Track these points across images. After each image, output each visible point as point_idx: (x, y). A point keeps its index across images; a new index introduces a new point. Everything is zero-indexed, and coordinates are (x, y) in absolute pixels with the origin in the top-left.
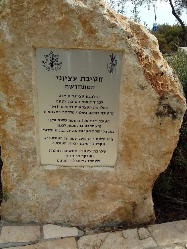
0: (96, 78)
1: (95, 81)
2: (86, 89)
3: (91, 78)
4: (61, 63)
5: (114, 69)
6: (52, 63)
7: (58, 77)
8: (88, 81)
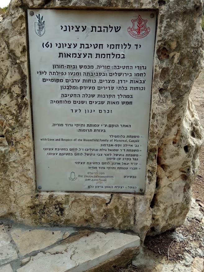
0: (96, 44)
1: (95, 48)
3: (91, 45)
4: (149, 28)
5: (42, 33)
6: (139, 28)
7: (62, 27)
8: (88, 48)
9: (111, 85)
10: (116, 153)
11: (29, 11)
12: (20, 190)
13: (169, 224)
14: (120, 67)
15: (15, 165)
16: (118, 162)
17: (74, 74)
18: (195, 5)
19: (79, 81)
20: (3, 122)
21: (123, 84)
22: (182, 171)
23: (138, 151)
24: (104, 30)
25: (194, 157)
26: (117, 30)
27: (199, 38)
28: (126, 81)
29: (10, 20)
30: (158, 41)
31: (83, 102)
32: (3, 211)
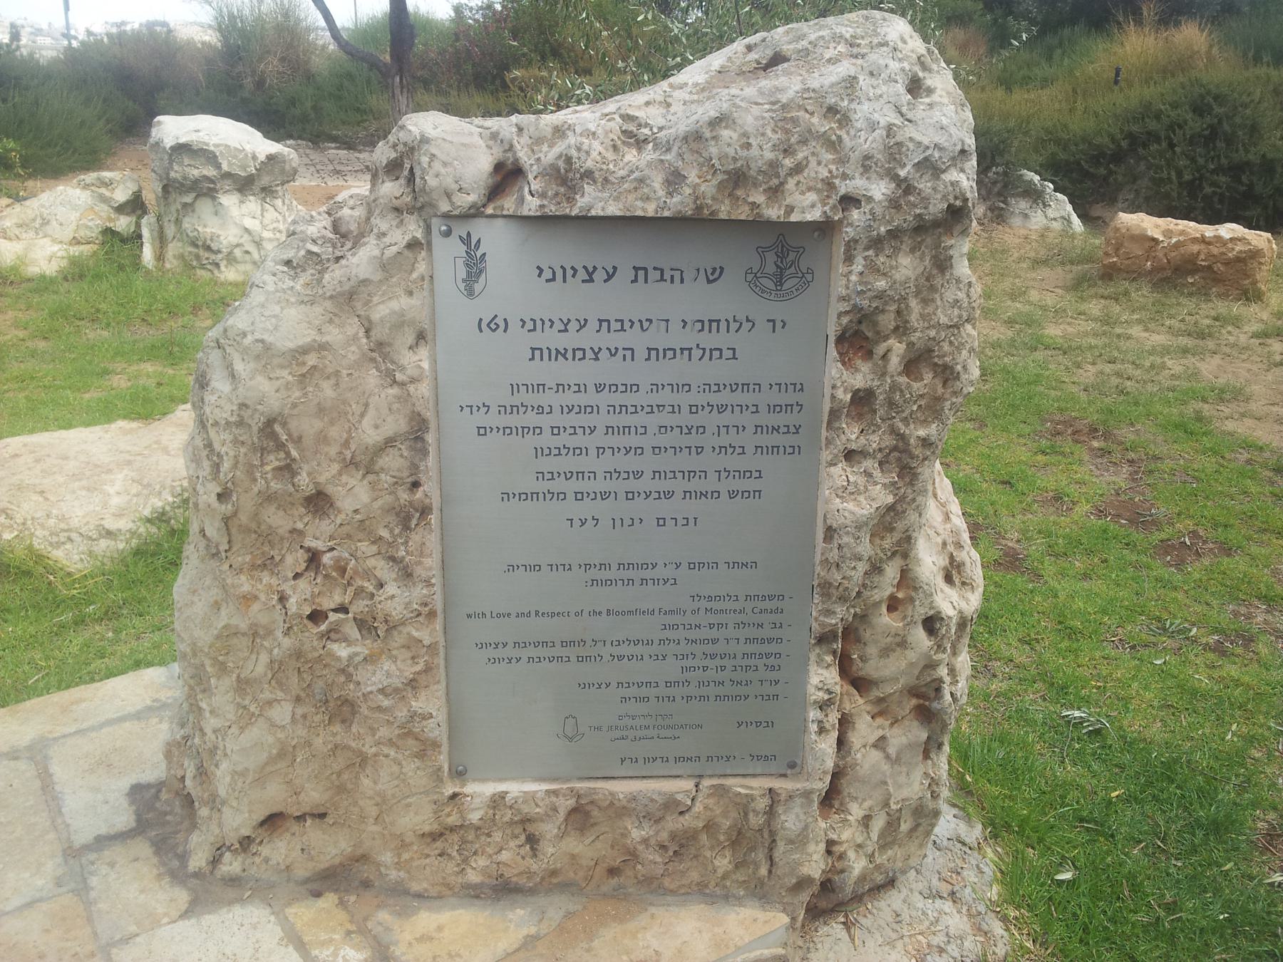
3: (575, 270)
9: (694, 440)
10: (710, 648)
12: (396, 782)
13: (878, 867)
15: (386, 703)
16: (721, 676)
19: (592, 432)
22: (917, 696)
26: (711, 278)
27: (961, 295)
29: (377, 252)
30: (840, 315)
31: (605, 496)
32: (334, 852)
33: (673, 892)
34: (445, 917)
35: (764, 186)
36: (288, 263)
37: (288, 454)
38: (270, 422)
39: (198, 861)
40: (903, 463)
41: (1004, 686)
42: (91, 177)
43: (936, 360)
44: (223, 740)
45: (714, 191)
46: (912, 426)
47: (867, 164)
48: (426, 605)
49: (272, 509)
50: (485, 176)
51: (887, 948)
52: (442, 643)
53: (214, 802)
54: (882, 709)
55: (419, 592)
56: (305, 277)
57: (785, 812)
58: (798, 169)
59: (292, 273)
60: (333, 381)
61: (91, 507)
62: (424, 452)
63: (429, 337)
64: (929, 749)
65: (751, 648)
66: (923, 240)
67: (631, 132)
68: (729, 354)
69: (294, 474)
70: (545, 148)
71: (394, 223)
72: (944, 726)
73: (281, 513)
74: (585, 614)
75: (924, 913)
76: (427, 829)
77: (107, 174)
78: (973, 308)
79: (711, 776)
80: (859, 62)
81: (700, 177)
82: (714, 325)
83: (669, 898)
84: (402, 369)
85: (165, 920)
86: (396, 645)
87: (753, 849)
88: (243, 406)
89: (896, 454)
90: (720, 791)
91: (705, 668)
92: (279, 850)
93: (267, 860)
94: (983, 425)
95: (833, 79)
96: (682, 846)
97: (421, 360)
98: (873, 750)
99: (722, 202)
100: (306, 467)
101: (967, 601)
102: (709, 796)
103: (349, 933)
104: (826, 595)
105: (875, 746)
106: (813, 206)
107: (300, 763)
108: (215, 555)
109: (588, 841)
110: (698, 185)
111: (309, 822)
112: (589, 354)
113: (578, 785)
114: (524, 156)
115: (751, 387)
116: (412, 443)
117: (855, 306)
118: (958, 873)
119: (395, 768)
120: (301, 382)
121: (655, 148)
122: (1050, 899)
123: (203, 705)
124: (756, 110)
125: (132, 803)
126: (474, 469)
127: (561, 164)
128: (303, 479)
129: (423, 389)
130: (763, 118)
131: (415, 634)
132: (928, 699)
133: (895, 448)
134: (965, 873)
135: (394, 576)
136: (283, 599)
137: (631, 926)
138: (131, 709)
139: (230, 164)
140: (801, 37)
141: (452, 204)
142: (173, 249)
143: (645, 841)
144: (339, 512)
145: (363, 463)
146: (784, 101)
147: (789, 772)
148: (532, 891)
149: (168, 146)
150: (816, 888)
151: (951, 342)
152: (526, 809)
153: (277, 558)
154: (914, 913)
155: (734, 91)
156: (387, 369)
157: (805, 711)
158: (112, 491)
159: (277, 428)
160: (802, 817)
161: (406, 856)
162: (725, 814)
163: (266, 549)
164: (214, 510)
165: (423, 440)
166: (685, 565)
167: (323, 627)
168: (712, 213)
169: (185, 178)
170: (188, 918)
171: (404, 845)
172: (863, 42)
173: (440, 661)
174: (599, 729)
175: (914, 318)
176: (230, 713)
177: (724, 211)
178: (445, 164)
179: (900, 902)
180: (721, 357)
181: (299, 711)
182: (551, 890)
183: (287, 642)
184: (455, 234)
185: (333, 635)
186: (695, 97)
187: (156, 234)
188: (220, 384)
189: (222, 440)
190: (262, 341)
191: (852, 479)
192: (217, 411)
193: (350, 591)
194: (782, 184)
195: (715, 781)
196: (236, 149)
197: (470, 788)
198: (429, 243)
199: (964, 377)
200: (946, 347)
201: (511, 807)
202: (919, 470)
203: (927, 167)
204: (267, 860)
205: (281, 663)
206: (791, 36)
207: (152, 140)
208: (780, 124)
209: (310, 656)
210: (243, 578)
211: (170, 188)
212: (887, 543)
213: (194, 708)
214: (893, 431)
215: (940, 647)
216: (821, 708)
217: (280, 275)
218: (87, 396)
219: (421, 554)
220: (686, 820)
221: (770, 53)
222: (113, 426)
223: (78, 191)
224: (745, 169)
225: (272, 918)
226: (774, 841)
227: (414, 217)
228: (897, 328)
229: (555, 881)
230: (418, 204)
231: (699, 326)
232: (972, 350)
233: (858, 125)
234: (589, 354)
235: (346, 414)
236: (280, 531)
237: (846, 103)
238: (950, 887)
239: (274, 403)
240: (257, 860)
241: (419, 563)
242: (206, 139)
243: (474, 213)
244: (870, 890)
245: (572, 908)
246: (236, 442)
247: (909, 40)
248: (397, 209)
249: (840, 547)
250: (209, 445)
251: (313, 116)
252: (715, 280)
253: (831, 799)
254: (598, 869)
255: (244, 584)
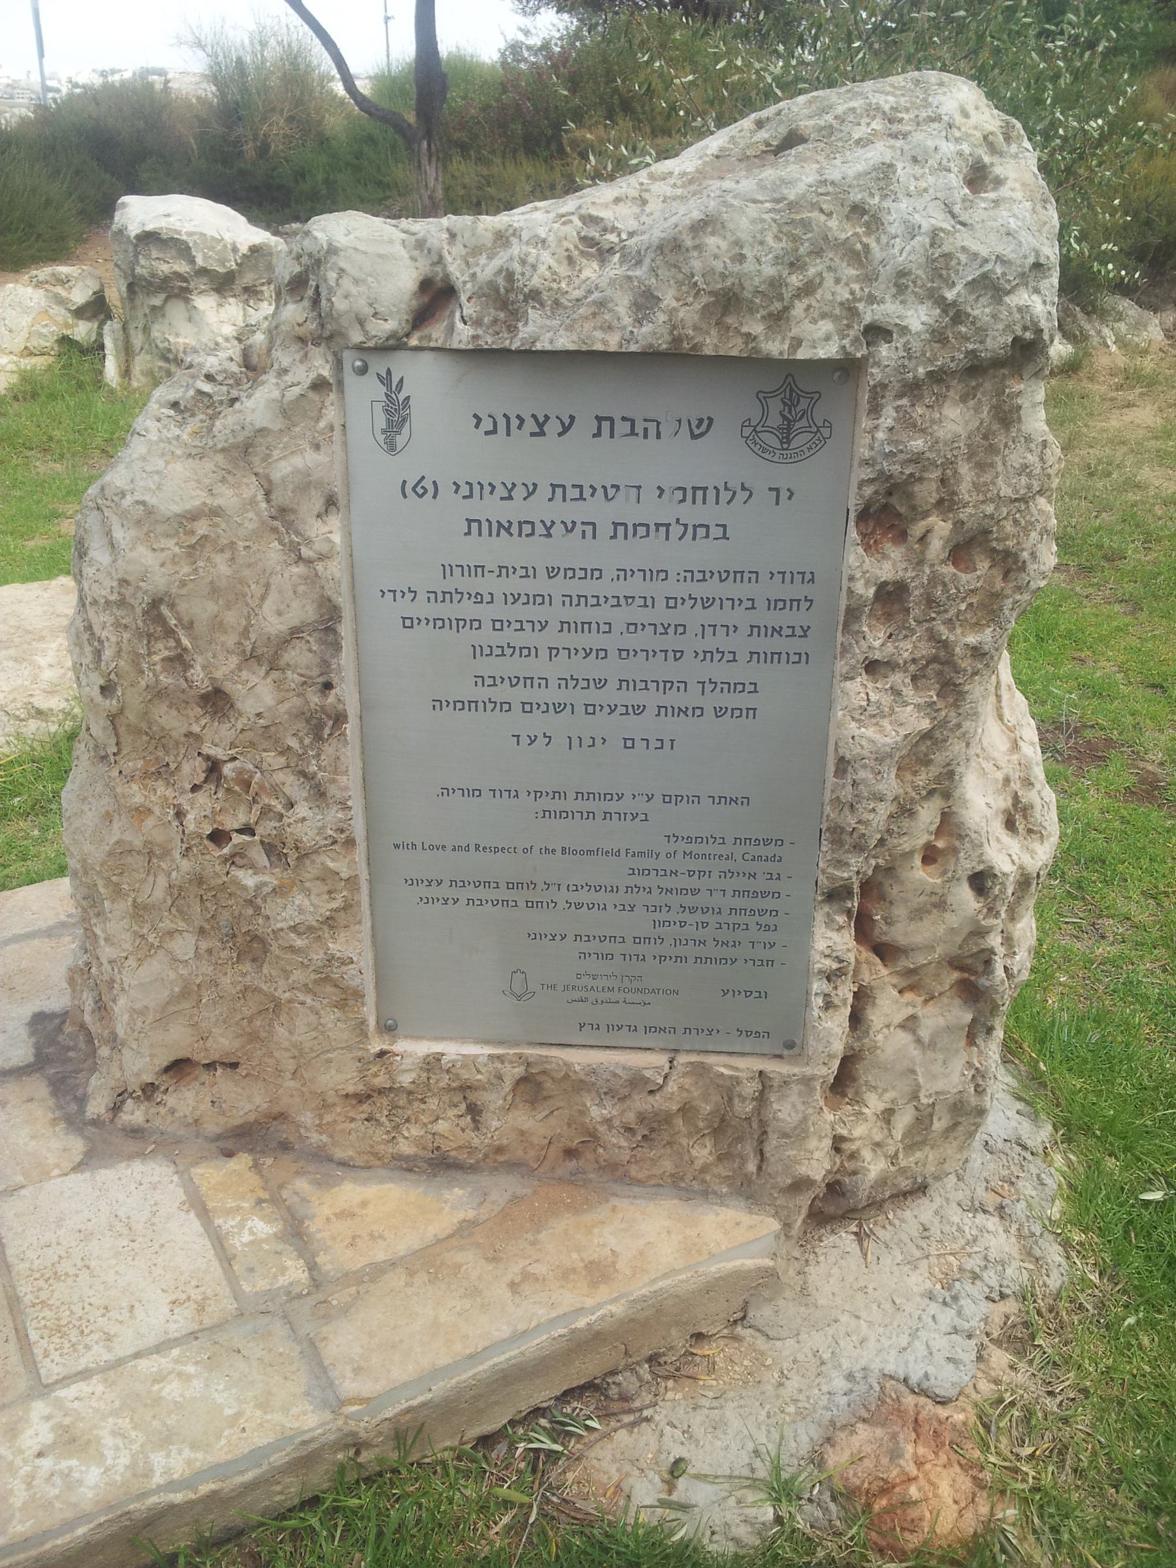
2: (694, 502)
3: (522, 420)
7: (479, 420)
9: (671, 642)
10: (688, 900)
11: (351, 360)
12: (314, 1034)
13: (903, 1171)
14: (708, 575)
15: (299, 943)
16: (700, 934)
17: (524, 599)
18: (1016, 340)
19: (543, 628)
20: (251, 777)
21: (719, 641)
22: (962, 969)
23: (777, 895)
24: (646, 430)
25: (1013, 917)
26: (697, 432)
27: (1032, 458)
28: (732, 629)
29: (276, 394)
30: (862, 484)
31: (559, 708)
32: (248, 1107)
33: (640, 1182)
34: (372, 1191)
35: (763, 312)
36: (175, 405)
37: (178, 641)
38: (156, 603)
39: (97, 1106)
40: (947, 679)
41: (1114, 950)
42: (44, 272)
43: (994, 544)
44: (120, 972)
45: (696, 317)
46: (959, 631)
47: (901, 282)
48: (342, 831)
49: (164, 708)
50: (407, 297)
51: (906, 1268)
52: (364, 875)
53: (114, 1041)
54: (912, 982)
55: (334, 815)
56: (194, 424)
57: (779, 1100)
58: (808, 289)
59: (179, 418)
60: (227, 555)
61: (20, 682)
62: (337, 647)
63: (342, 502)
64: (974, 1033)
65: (739, 902)
66: (979, 385)
67: (592, 239)
68: (716, 532)
69: (187, 666)
70: (483, 260)
71: (298, 357)
72: (994, 1009)
73: (174, 713)
74: (536, 850)
75: (959, 1230)
76: (351, 1089)
77: (63, 270)
78: (1049, 476)
79: (689, 1051)
80: (899, 143)
81: (678, 300)
82: (700, 494)
83: (636, 1189)
84: (309, 542)
85: (56, 1172)
86: (308, 876)
87: (739, 1139)
88: (124, 582)
89: (936, 666)
90: (699, 1070)
91: (683, 924)
92: (185, 1100)
93: (172, 1111)
94: (1137, 608)
95: (860, 167)
96: (652, 1130)
97: (328, 532)
98: (899, 1031)
99: (708, 333)
100: (200, 660)
101: (1032, 853)
102: (685, 1074)
103: (260, 1201)
104: (837, 842)
105: (902, 1026)
106: (827, 338)
107: (206, 1005)
108: (104, 758)
109: (539, 1117)
110: (677, 310)
111: (220, 1071)
112: (540, 529)
113: (529, 1051)
114: (456, 270)
115: (746, 576)
116: (322, 635)
117: (881, 472)
118: (1012, 1183)
119: (313, 1018)
120: (189, 555)
121: (622, 262)
122: (1130, 1222)
123: (98, 931)
124: (752, 210)
125: (32, 1034)
126: (395, 667)
127: (501, 281)
128: (197, 673)
129: (334, 569)
130: (763, 221)
131: (331, 865)
132: (975, 973)
133: (934, 659)
134: (1020, 1183)
135: (305, 794)
136: (180, 814)
137: (588, 1218)
138: (42, 925)
139: (206, 257)
140: (825, 110)
141: (366, 333)
142: (140, 364)
143: (608, 1121)
144: (240, 714)
145: (266, 656)
146: (792, 197)
147: (786, 1052)
148: (473, 1169)
149: (133, 234)
150: (821, 1190)
151: (1016, 521)
152: (464, 1075)
153: (173, 766)
154: (947, 1229)
155: (728, 184)
156: (291, 542)
157: (809, 983)
158: (42, 661)
159: (165, 610)
160: (800, 1107)
161: (328, 1118)
162: (705, 1097)
163: (160, 754)
164: (96, 705)
165: (335, 632)
166: (658, 798)
167: (226, 850)
168: (694, 347)
169: (153, 275)
170: (82, 1172)
171: (326, 1106)
172: (906, 117)
173: (364, 896)
174: (553, 987)
175: (964, 490)
176: (126, 941)
177: (710, 344)
178: (356, 282)
179: (930, 1213)
180: (707, 536)
181: (204, 945)
182: (496, 1169)
183: (185, 865)
184: (372, 371)
185: (237, 859)
186: (679, 192)
187: (120, 343)
188: (99, 554)
189: (101, 620)
190: (143, 503)
191: (874, 697)
192: (95, 586)
193: (256, 809)
194: (786, 309)
195: (694, 1058)
196: (213, 238)
197: (400, 1046)
198: (340, 383)
199: (1032, 567)
200: (1009, 527)
201: (448, 1071)
202: (967, 688)
203: (985, 288)
204: (172, 1111)
205: (180, 888)
206: (814, 107)
207: (114, 227)
208: (785, 229)
209: (213, 883)
210: (135, 787)
211: (135, 286)
212: (922, 779)
213: (89, 934)
214: (933, 636)
215: (992, 911)
216: (829, 979)
217: (165, 421)
218: (31, 544)
219: (336, 772)
220: (657, 1101)
221: (783, 130)
222: (54, 583)
223: (30, 290)
224: (737, 289)
225: (175, 1178)
226: (765, 1132)
227: (322, 349)
228: (941, 502)
229: (501, 1158)
230: (325, 334)
231: (679, 495)
232: (1045, 531)
233: (892, 230)
234: (540, 529)
235: (244, 596)
236: (173, 733)
237: (877, 200)
238: (999, 1199)
239: (159, 581)
240: (162, 1110)
241: (334, 781)
242: (178, 226)
243: (394, 345)
244: (892, 1196)
245: (521, 1191)
246: (117, 625)
247: (972, 112)
248: (301, 340)
249: (854, 783)
250: (89, 628)
251: (324, 192)
252: (702, 435)
253: (844, 1082)
254: (552, 1148)
255: (136, 794)
